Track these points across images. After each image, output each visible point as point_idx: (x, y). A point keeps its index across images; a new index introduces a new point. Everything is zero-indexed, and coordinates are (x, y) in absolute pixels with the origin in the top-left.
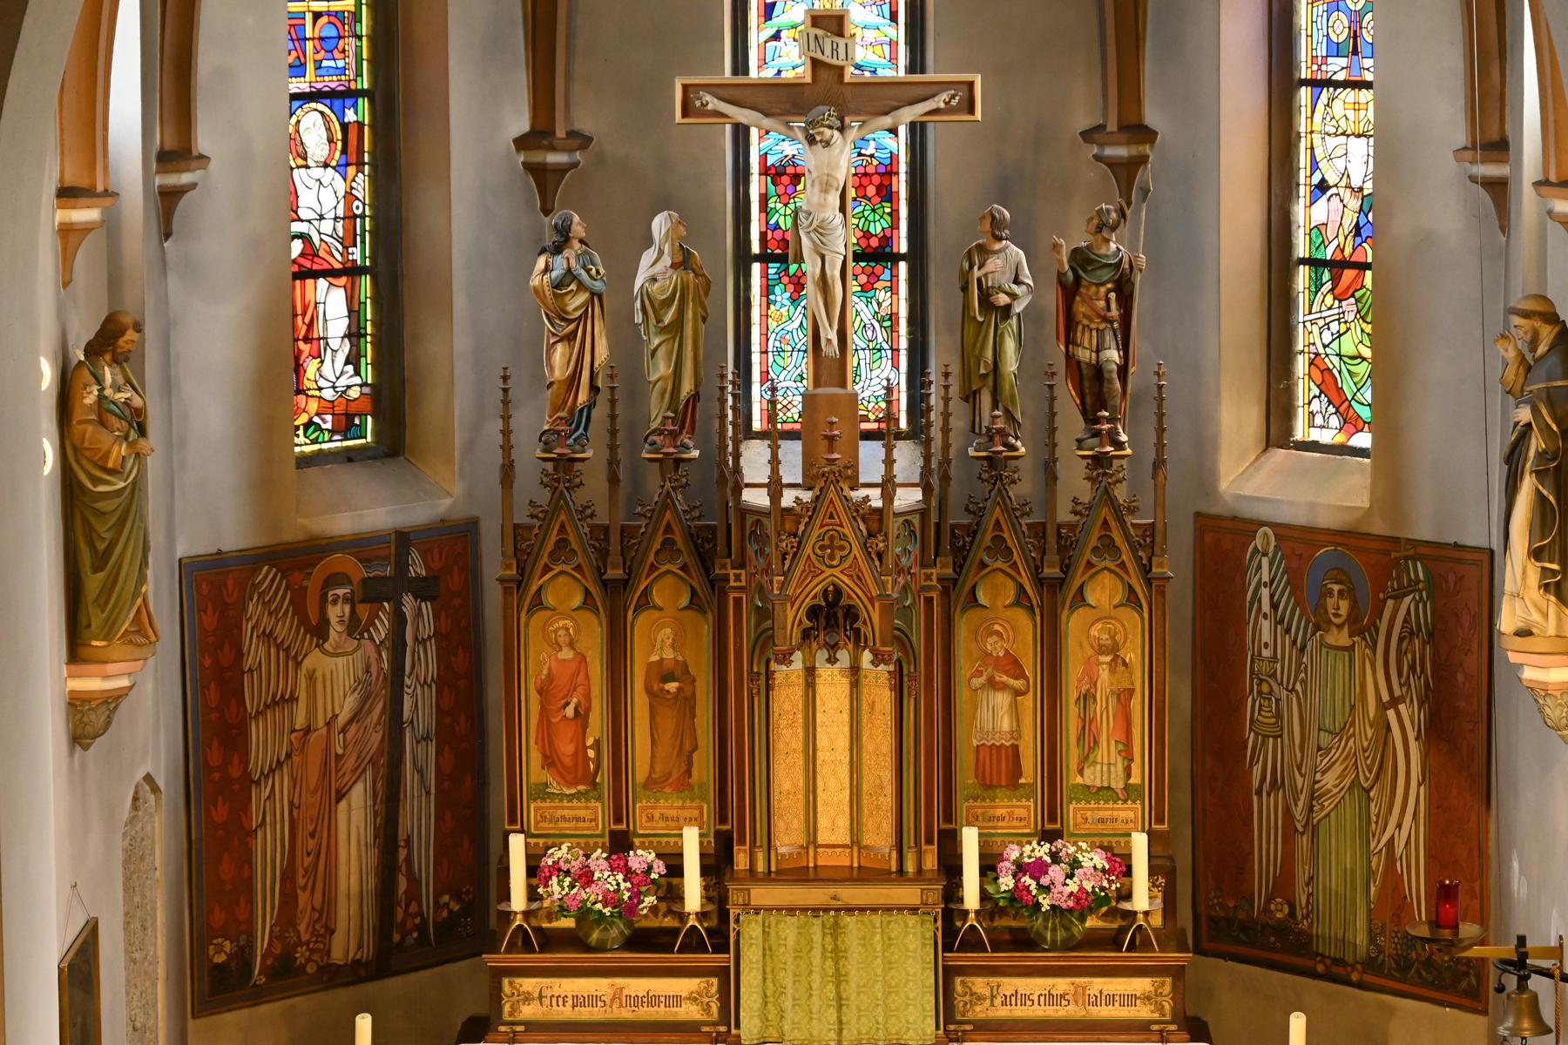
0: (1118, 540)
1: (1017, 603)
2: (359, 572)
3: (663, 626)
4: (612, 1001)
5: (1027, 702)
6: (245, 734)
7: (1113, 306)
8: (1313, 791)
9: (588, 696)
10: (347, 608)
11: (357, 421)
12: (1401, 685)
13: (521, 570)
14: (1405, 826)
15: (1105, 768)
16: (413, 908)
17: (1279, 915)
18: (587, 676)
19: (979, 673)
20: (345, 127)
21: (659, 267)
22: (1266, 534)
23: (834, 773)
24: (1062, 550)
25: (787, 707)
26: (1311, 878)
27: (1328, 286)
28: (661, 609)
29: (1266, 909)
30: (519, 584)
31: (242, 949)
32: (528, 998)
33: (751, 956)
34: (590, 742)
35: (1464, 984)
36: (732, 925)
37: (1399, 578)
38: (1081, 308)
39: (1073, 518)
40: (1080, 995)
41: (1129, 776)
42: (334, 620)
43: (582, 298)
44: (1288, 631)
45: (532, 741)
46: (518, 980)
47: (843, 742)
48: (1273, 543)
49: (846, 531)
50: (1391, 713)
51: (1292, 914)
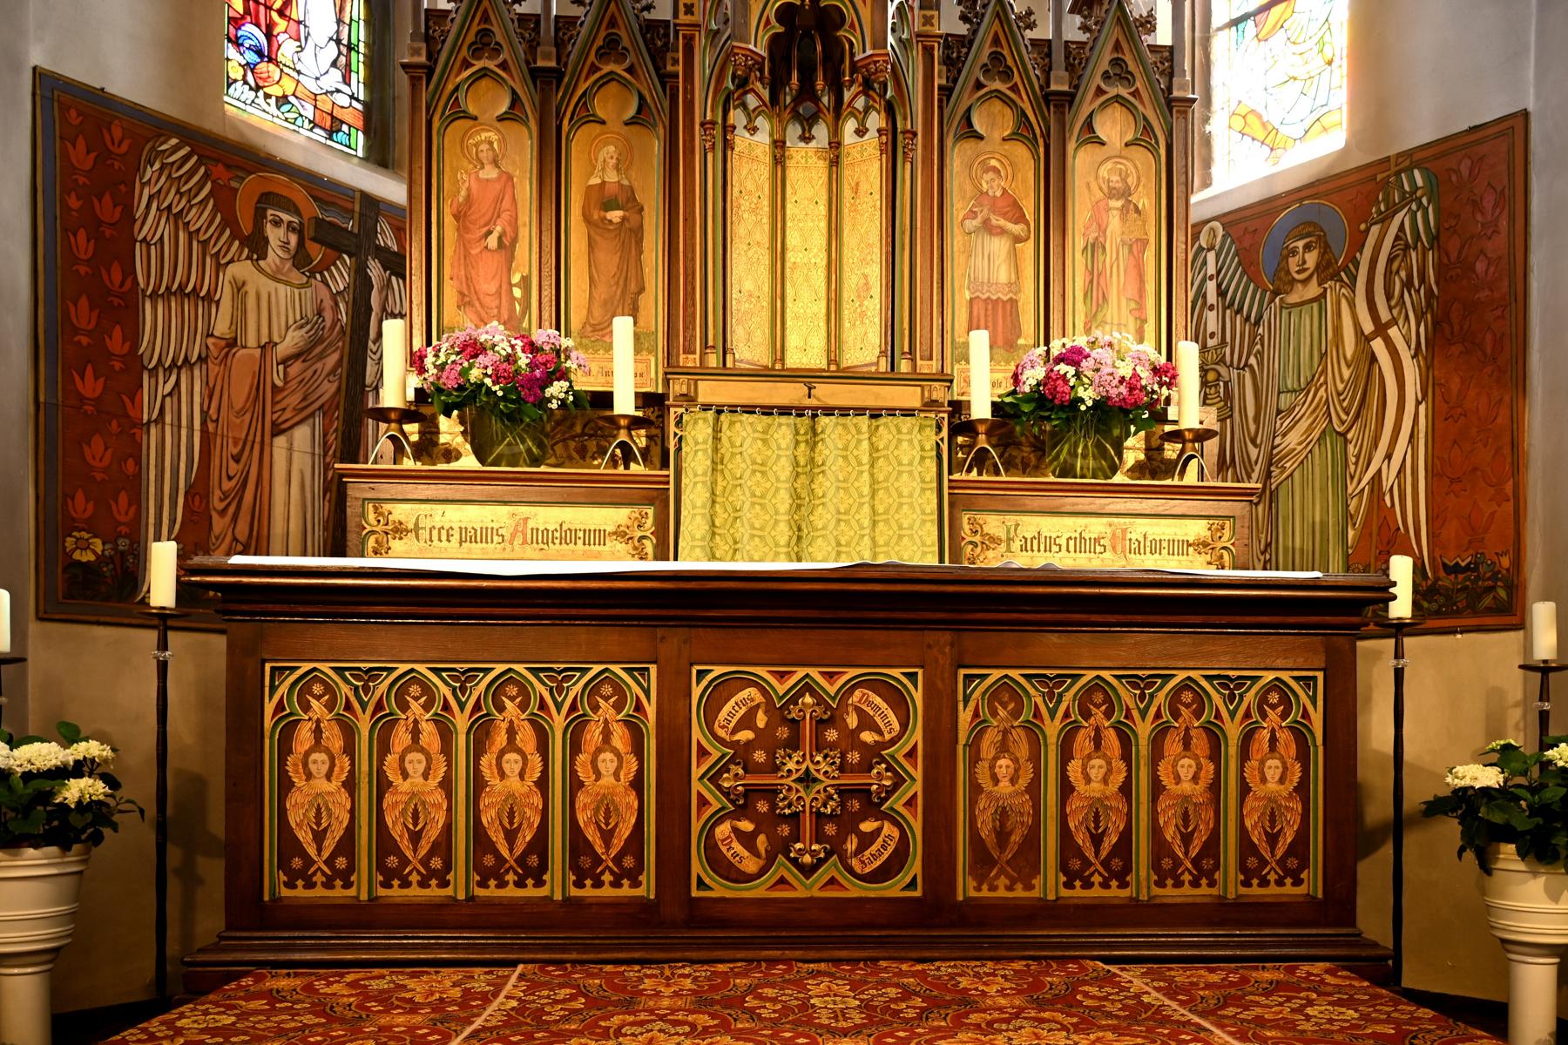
1: (1014, 137)
2: (312, 210)
4: (513, 536)
5: (1028, 249)
8: (1271, 456)
10: (293, 239)
11: (345, 128)
12: (1390, 309)
13: (432, 56)
18: (514, 200)
19: (972, 214)
23: (807, 279)
24: (1070, 67)
25: (750, 185)
26: (1268, 545)
28: (603, 122)
33: (696, 463)
34: (516, 278)
35: (1488, 601)
36: (672, 428)
39: (1083, 37)
44: (1239, 311)
47: (819, 240)
48: (1220, 232)
50: (1378, 345)
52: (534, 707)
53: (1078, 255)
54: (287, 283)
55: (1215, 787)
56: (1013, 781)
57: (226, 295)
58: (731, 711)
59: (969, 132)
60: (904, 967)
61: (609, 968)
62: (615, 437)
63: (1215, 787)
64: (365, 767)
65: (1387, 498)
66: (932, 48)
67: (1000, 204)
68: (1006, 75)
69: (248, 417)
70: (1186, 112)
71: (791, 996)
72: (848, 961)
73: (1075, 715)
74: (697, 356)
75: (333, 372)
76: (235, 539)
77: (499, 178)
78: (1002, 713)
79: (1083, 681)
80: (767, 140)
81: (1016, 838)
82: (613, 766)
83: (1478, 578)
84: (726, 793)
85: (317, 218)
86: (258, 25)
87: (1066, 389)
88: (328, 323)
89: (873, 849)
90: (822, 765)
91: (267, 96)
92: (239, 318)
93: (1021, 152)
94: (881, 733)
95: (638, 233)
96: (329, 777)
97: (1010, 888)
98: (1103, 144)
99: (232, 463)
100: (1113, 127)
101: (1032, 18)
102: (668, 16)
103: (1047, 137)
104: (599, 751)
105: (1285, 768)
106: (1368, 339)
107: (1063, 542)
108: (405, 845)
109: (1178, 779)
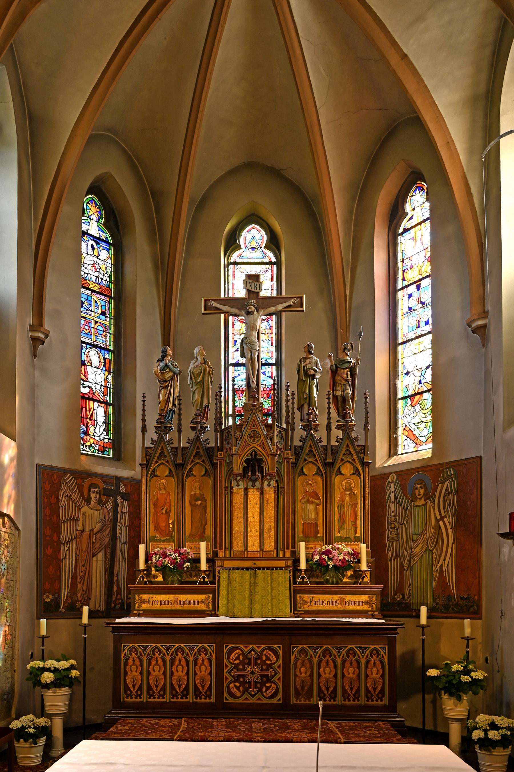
0: (352, 451)
2: (102, 485)
3: (196, 482)
5: (321, 508)
6: (59, 527)
7: (349, 376)
8: (411, 555)
9: (170, 506)
10: (98, 496)
11: (107, 450)
12: (445, 512)
14: (448, 561)
16: (119, 596)
17: (398, 599)
20: (105, 359)
21: (196, 364)
22: (393, 476)
24: (333, 454)
26: (410, 585)
27: (410, 403)
29: (394, 598)
30: (147, 466)
31: (56, 598)
32: (144, 602)
33: (223, 584)
34: (171, 522)
35: (472, 610)
36: (217, 574)
37: (443, 476)
38: (338, 378)
39: (337, 444)
40: (342, 602)
41: (356, 533)
42: (93, 498)
43: (171, 374)
44: (401, 505)
45: (151, 522)
46: (141, 595)
47: (257, 515)
48: (395, 478)
49: (259, 430)
50: (441, 523)
51: (403, 598)
52: (185, 654)
53: (336, 509)
54: (96, 510)
55: (359, 676)
56: (306, 673)
57: (81, 518)
58: (233, 655)
59: (302, 473)
60: (276, 720)
61: (204, 719)
62: (202, 574)
63: (359, 676)
64: (145, 669)
65: (444, 573)
69: (86, 553)
71: (248, 726)
72: (263, 719)
73: (321, 657)
75: (108, 535)
76: (83, 590)
77: (165, 493)
78: (302, 656)
79: (323, 648)
80: (243, 487)
81: (306, 688)
82: (204, 669)
83: (469, 602)
84: (232, 676)
85: (104, 488)
86: (84, 425)
87: (325, 562)
88: (107, 520)
89: (270, 690)
90: (256, 669)
91: (86, 446)
92: (84, 525)
93: (319, 478)
94: (271, 661)
95: (205, 508)
96: (136, 671)
97: (305, 701)
98: (343, 475)
99: (82, 568)
100: (347, 470)
102: (214, 445)
103: (326, 474)
104: (201, 665)
105: (378, 670)
106: (439, 521)
107: (326, 602)
108: (154, 688)
109: (349, 673)
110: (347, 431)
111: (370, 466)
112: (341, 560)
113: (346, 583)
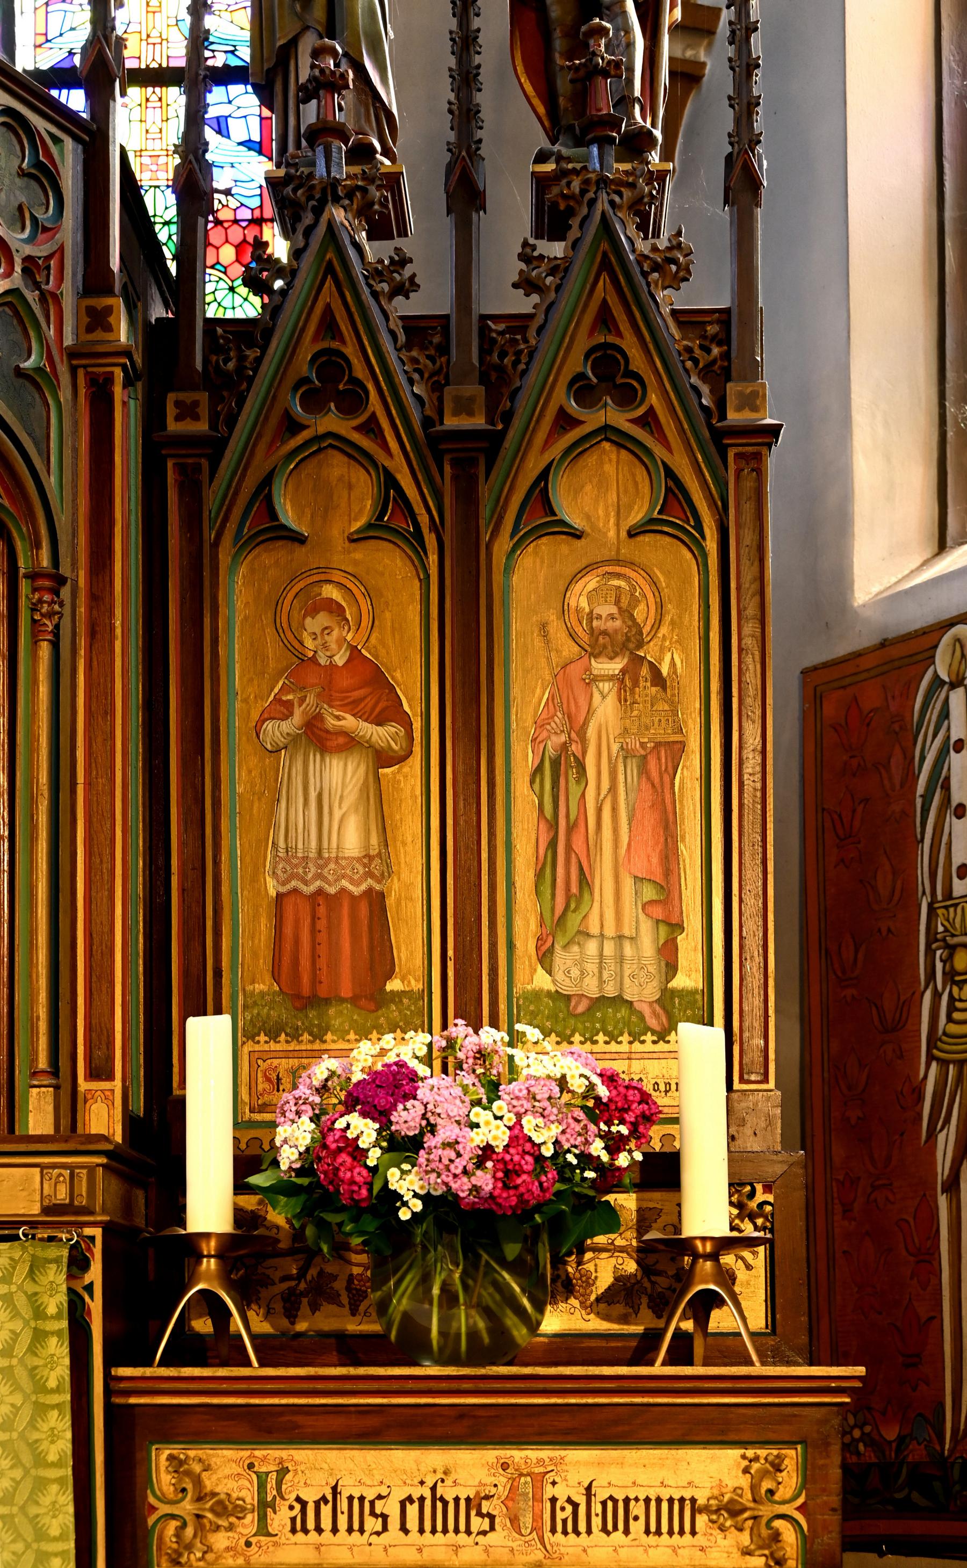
5: (408, 779)
15: (612, 947)
19: (283, 710)
39: (523, 304)
41: (671, 968)
66: (110, 378)
67: (345, 681)
68: (352, 401)
70: (758, 458)
74: (117, 1084)
87: (360, 1175)
93: (390, 564)
98: (577, 535)
101: (408, 271)
107: (393, 1510)
110: (603, 204)
111: (774, 461)
112: (488, 1150)
113: (569, 1348)
